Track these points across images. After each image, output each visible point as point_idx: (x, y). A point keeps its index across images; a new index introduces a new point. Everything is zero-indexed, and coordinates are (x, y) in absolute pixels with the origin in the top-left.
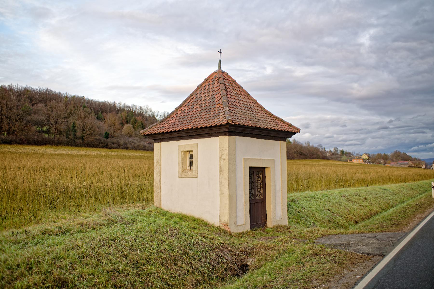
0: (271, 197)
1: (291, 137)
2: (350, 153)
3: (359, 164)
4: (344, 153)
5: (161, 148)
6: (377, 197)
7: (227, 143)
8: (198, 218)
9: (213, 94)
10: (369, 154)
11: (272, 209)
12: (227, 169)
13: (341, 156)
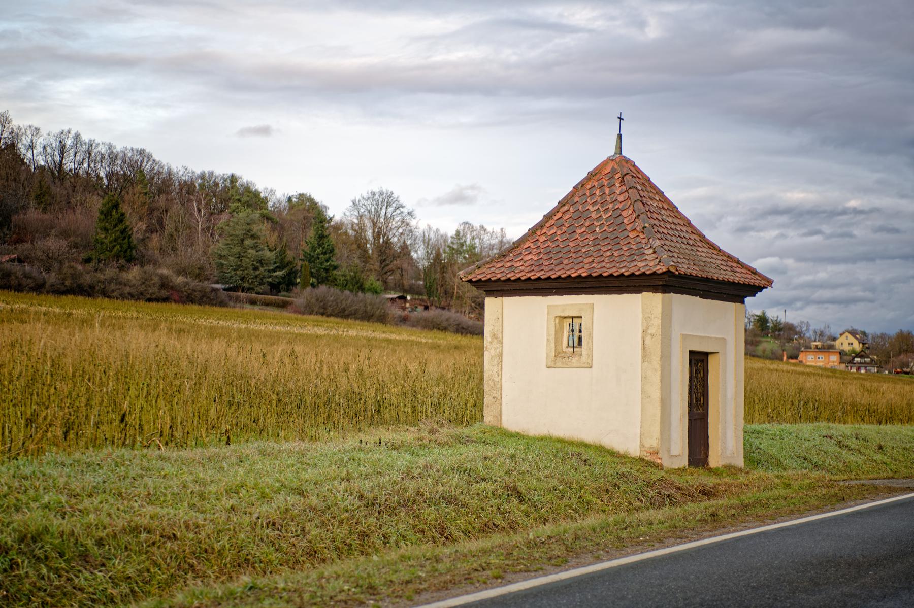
0: (718, 411)
1: (754, 296)
2: (790, 328)
3: (826, 369)
4: (770, 325)
5: (502, 308)
6: (908, 447)
7: (660, 306)
8: (592, 443)
9: (616, 207)
10: (864, 334)
11: (720, 434)
12: (659, 352)
13: (758, 339)
